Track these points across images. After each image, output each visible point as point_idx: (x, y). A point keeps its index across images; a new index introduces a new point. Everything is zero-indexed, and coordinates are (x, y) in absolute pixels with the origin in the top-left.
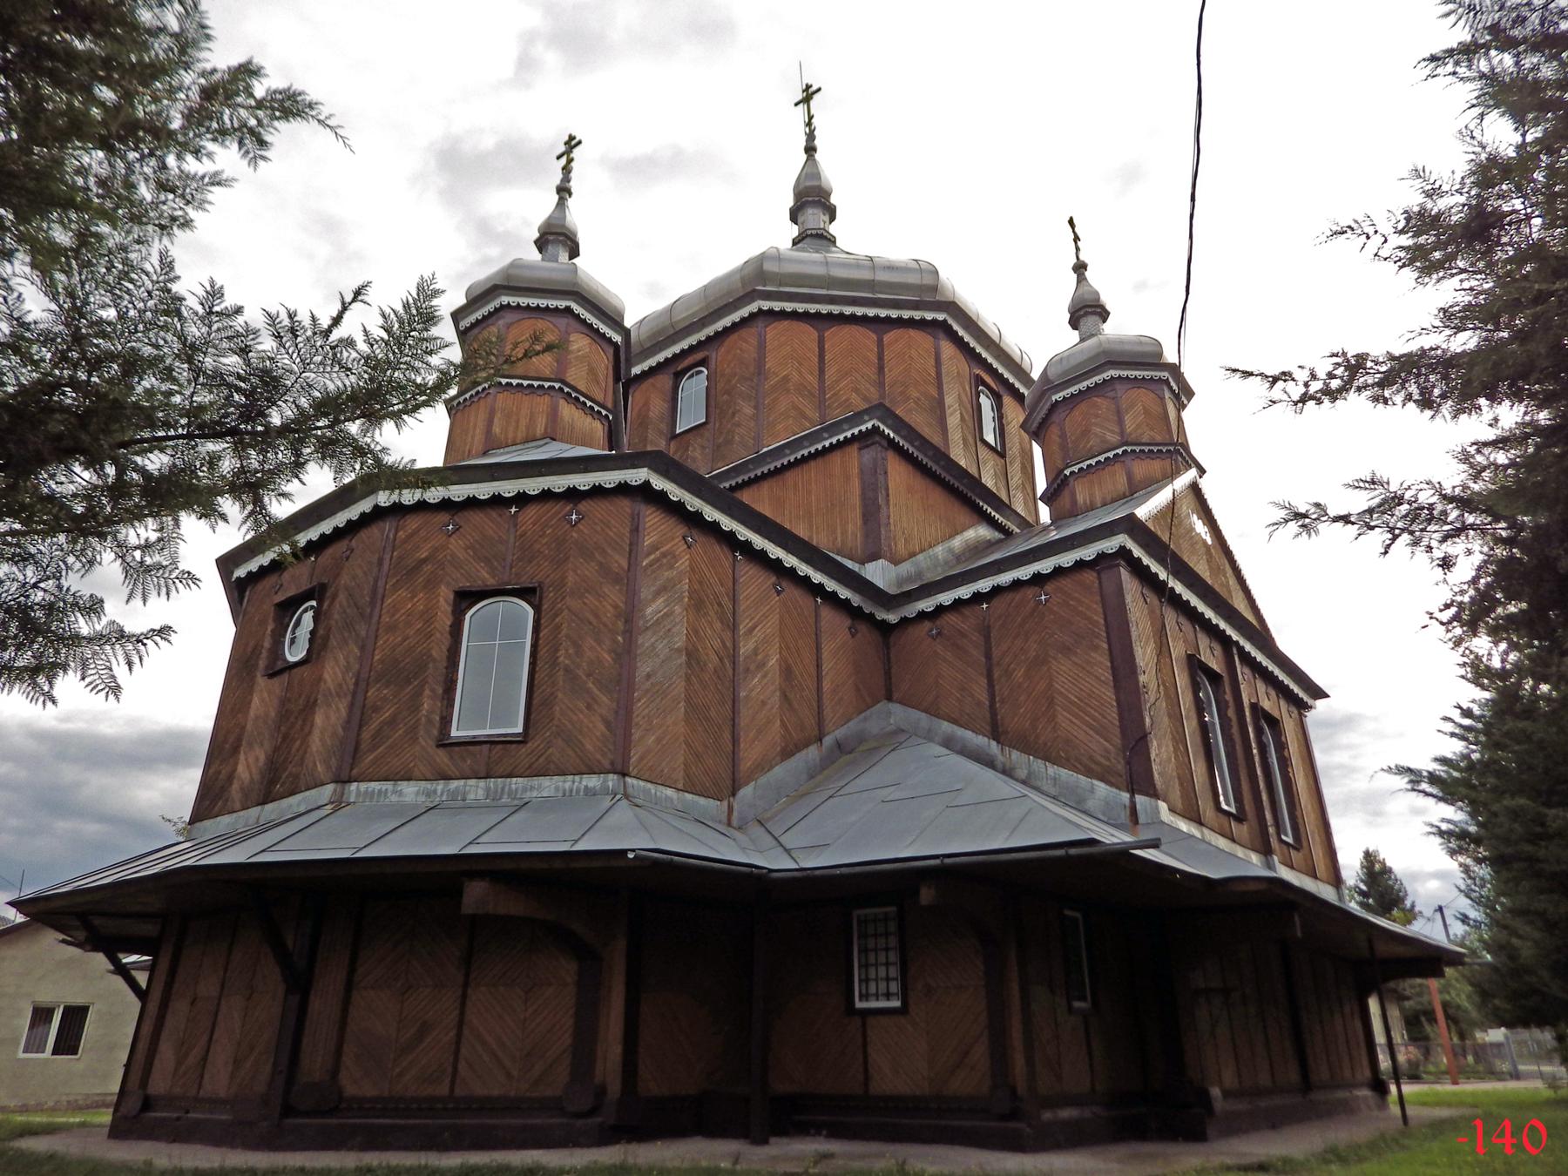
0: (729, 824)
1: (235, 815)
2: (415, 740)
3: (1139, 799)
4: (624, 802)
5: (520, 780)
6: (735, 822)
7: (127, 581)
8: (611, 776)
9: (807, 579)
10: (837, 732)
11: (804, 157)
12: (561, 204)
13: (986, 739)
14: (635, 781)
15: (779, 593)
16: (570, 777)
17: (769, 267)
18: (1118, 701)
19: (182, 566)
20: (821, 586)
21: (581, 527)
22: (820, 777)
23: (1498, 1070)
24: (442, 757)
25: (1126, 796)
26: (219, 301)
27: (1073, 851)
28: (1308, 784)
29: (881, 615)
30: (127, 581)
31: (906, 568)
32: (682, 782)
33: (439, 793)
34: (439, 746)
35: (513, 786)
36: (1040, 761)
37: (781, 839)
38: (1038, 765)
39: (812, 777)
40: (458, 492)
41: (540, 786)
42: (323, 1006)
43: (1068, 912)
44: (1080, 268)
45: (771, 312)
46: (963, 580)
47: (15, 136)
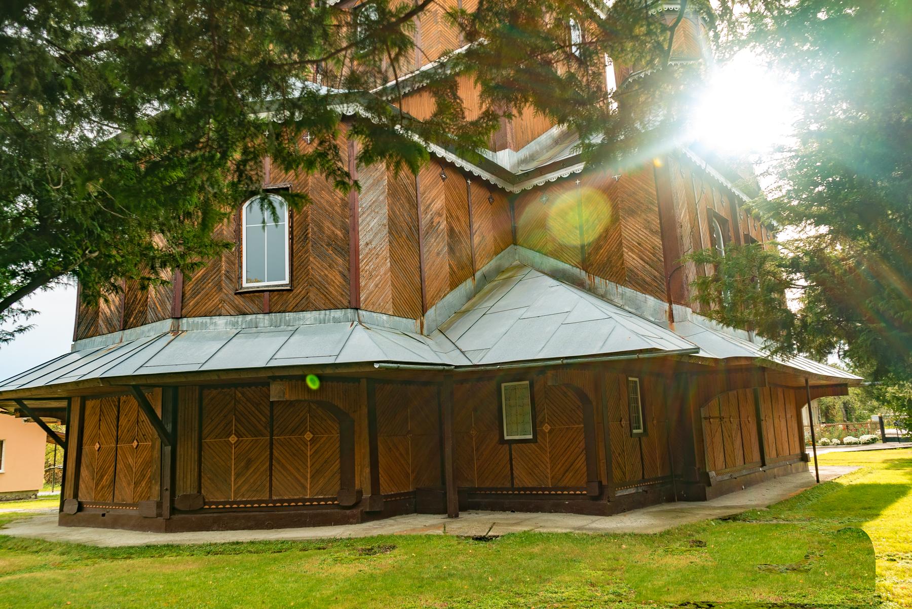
0: (422, 334)
1: (104, 336)
2: (221, 289)
3: (674, 306)
4: (360, 327)
5: (291, 314)
6: (425, 332)
8: (349, 310)
9: (462, 168)
10: (483, 269)
13: (578, 270)
14: (364, 312)
15: (443, 179)
16: (323, 312)
18: (663, 245)
20: (471, 172)
22: (474, 300)
24: (239, 301)
25: (666, 306)
27: (641, 356)
29: (509, 188)
31: (524, 153)
32: (392, 310)
33: (240, 324)
34: (236, 294)
35: (287, 318)
36: (613, 283)
37: (457, 344)
38: (611, 286)
39: (469, 299)
41: (304, 317)
42: (187, 452)
43: (630, 379)
46: (563, 165)
47: (117, 95)
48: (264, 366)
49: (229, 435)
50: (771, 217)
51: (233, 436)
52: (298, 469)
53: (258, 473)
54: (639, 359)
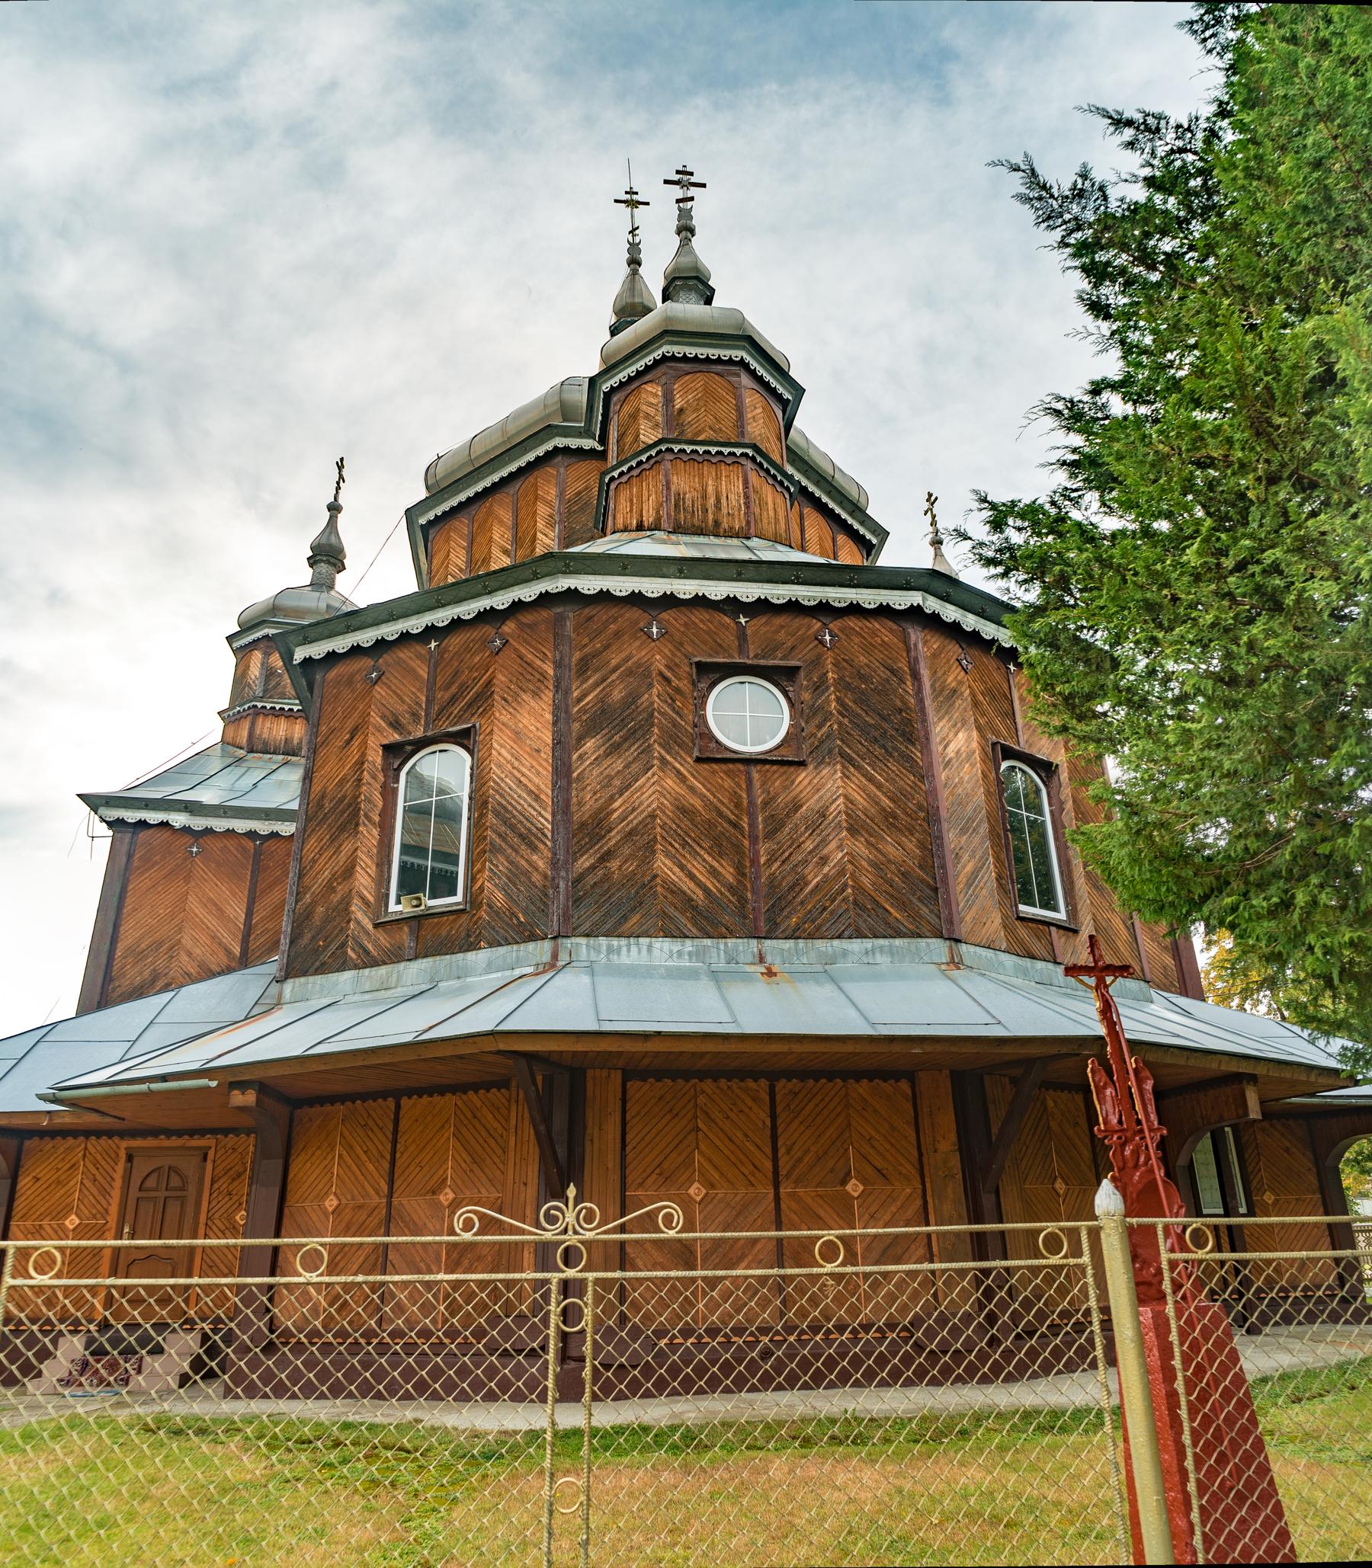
7: (478, 1185)
11: (676, 240)
12: (685, 243)
14: (972, 949)
17: (288, 602)
19: (1078, 395)
21: (756, 776)
23: (306, 1170)
26: (453, 983)
27: (155, 1086)
28: (686, 321)
30: (478, 1185)
40: (441, 617)
44: (334, 508)
45: (566, 450)
48: (489, 1027)
49: (844, 1182)
50: (1260, 61)
51: (854, 1181)
52: (351, 1147)
53: (512, 1154)
54: (151, 1092)
